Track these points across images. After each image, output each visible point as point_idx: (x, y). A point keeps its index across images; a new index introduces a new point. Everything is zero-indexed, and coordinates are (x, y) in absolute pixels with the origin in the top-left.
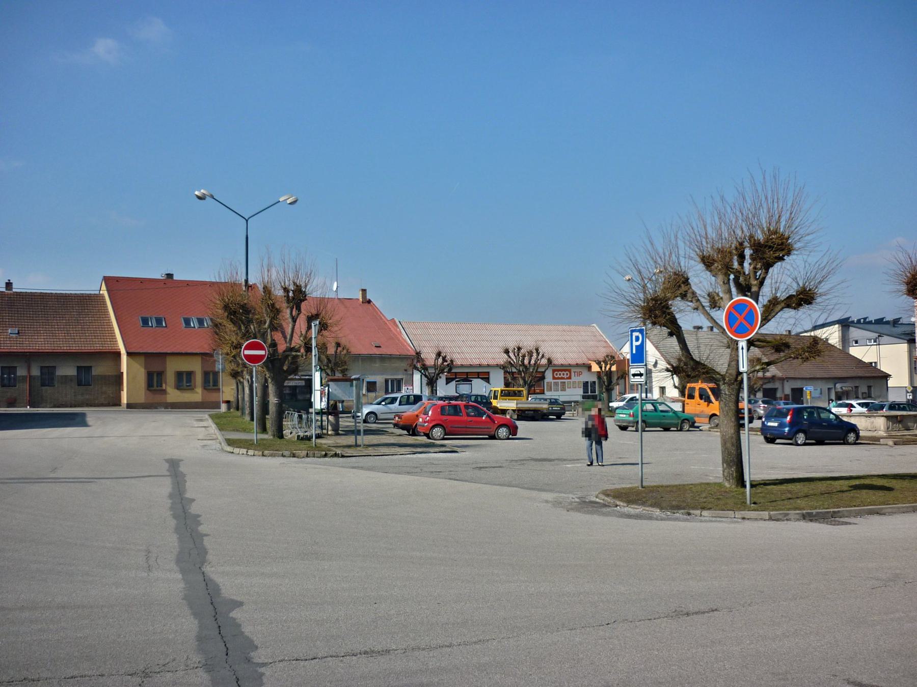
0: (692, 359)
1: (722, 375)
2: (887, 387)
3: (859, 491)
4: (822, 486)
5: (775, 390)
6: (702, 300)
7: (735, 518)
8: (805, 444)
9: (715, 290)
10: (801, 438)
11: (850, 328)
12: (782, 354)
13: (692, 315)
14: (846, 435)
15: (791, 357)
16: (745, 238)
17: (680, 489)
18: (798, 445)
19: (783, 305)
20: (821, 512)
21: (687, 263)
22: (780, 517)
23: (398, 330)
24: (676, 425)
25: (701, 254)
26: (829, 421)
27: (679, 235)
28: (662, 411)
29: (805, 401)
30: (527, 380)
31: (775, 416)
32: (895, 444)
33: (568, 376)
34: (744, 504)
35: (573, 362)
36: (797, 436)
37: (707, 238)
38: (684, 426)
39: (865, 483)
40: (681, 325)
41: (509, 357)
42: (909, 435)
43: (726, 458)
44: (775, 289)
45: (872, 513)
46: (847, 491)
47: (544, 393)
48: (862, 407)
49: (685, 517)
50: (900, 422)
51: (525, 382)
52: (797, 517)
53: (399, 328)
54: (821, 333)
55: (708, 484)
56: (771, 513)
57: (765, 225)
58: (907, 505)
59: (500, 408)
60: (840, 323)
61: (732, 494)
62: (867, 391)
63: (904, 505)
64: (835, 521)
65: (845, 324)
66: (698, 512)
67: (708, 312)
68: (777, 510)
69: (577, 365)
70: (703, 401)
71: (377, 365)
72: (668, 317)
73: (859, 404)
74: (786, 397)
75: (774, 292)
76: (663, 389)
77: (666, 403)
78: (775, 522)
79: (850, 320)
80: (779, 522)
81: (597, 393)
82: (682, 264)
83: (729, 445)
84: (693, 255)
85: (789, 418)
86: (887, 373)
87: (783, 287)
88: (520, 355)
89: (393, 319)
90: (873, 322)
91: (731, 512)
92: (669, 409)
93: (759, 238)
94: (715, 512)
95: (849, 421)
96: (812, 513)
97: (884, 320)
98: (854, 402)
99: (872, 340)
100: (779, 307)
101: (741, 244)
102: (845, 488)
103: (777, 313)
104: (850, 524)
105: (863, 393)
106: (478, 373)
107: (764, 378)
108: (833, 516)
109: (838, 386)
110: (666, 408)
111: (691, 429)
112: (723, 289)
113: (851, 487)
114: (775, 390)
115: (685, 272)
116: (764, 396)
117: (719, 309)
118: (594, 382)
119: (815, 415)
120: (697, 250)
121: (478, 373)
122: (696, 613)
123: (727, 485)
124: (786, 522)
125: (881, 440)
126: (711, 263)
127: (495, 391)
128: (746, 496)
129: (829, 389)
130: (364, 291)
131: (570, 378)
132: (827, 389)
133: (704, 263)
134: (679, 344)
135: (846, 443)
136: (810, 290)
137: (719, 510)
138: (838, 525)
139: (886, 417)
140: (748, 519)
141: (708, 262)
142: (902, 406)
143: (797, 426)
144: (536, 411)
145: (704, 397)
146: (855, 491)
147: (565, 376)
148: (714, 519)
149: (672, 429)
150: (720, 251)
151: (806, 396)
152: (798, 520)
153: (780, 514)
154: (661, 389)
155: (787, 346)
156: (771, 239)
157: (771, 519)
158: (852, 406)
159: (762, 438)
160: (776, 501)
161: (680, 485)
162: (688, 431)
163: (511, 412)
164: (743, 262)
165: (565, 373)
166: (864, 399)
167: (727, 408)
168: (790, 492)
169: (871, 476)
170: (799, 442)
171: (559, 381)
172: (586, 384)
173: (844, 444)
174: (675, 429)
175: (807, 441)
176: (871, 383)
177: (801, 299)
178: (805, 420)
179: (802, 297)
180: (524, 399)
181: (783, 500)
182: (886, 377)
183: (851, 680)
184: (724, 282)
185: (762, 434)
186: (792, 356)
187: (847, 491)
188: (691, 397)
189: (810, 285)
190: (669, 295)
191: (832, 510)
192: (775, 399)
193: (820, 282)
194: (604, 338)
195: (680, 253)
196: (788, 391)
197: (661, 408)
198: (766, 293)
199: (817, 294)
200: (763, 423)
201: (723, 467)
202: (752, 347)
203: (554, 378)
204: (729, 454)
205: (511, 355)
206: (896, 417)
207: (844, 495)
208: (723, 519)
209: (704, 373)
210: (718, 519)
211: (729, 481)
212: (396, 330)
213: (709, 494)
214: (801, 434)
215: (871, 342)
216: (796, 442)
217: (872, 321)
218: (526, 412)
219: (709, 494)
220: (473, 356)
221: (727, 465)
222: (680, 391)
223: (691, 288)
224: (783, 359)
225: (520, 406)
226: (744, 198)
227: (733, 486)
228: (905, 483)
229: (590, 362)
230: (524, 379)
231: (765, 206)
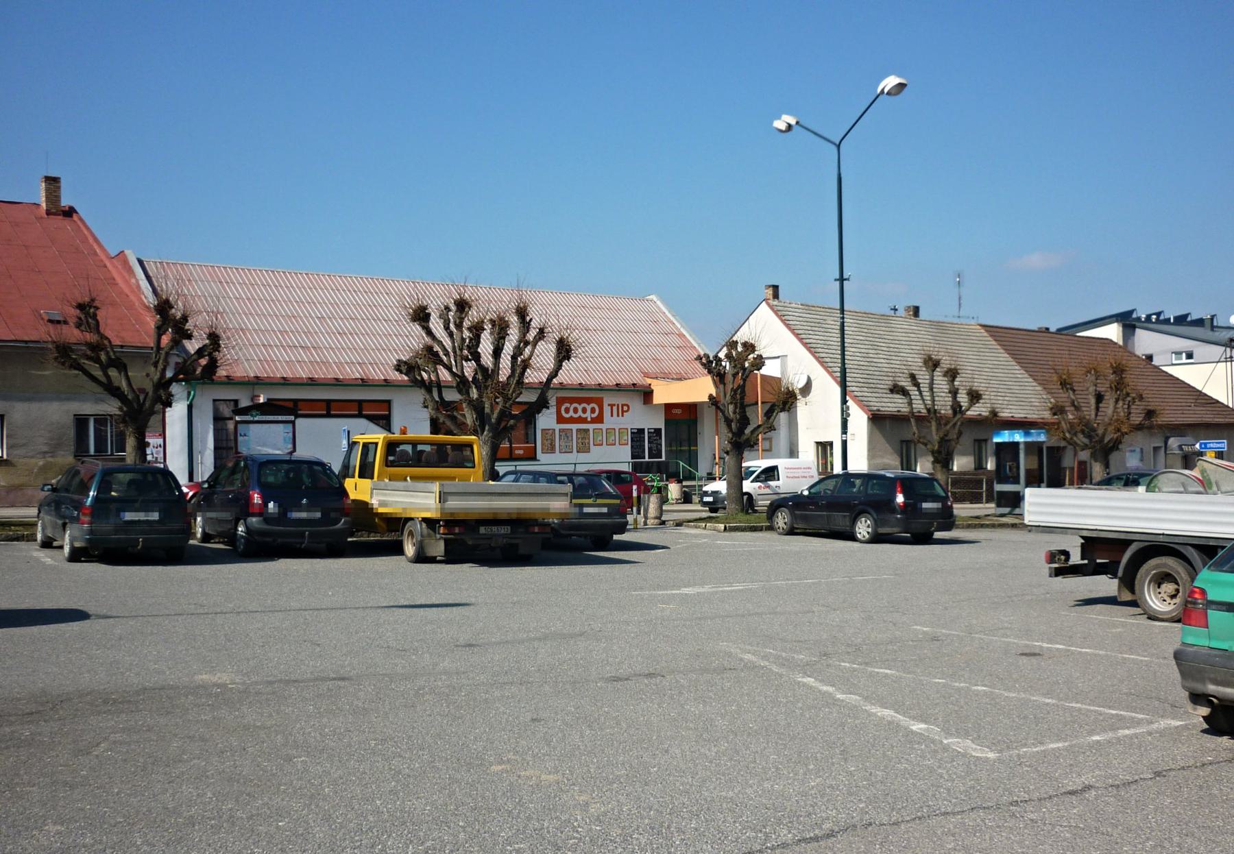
11: (1138, 331)
23: (133, 281)
30: (487, 410)
33: (594, 415)
35: (609, 381)
41: (429, 333)
47: (534, 458)
51: (482, 418)
53: (135, 276)
59: (381, 510)
60: (1121, 321)
69: (619, 388)
71: (47, 373)
79: (1134, 316)
81: (663, 459)
88: (466, 324)
89: (123, 252)
90: (1172, 321)
97: (1189, 319)
99: (1184, 355)
106: (360, 402)
118: (658, 431)
121: (360, 403)
127: (366, 446)
129: (1156, 449)
130: (52, 182)
131: (599, 419)
132: (1152, 449)
144: (519, 522)
147: (588, 415)
154: (977, 444)
163: (419, 528)
165: (589, 408)
171: (574, 427)
172: (638, 435)
180: (475, 476)
194: (677, 328)
203: (560, 419)
205: (436, 325)
212: (127, 282)
215: (1181, 359)
218: (482, 530)
220: (345, 357)
225: (454, 504)
229: (649, 381)
230: (477, 407)
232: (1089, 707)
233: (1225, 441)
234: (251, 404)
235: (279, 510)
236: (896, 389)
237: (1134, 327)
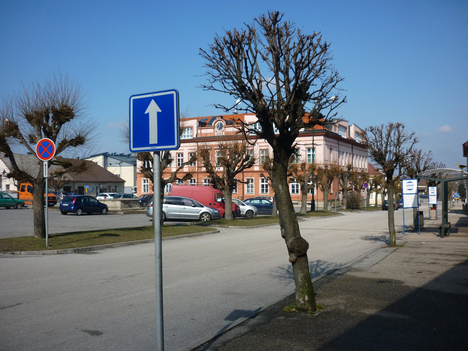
0: (19, 170)
1: (35, 179)
2: (124, 187)
3: (103, 237)
4: (86, 235)
5: (70, 187)
6: (25, 138)
7: (39, 254)
8: (82, 215)
9: (33, 133)
10: (80, 212)
11: (108, 157)
12: (68, 169)
13: (19, 146)
14: (102, 210)
15: (72, 171)
16: (49, 107)
17: (10, 240)
18: (78, 215)
19: (68, 143)
20: (83, 248)
21: (17, 117)
22: (63, 252)
24: (13, 206)
25: (26, 113)
26: (94, 203)
27: (13, 101)
28: (5, 198)
29: (85, 193)
31: (67, 201)
32: (124, 214)
34: (44, 247)
36: (78, 211)
37: (29, 105)
38: (18, 206)
39: (107, 233)
40: (12, 151)
42: (131, 209)
43: (36, 223)
44: (66, 135)
45: (108, 247)
46: (97, 237)
48: (111, 196)
49: (11, 255)
50: (127, 203)
52: (72, 251)
54: (95, 160)
55: (26, 237)
56: (58, 250)
57: (60, 102)
58: (124, 243)
61: (39, 242)
62: (115, 189)
63: (123, 243)
64: (90, 252)
65: (106, 155)
66: (18, 252)
67: (29, 145)
68: (62, 249)
70: (29, 193)
72: (5, 146)
73: (110, 195)
74: (76, 191)
75: (64, 137)
76: (8, 186)
77: (8, 194)
78: (60, 255)
79: (108, 153)
80: (62, 255)
82: (14, 118)
83: (38, 216)
84: (21, 113)
85: (74, 201)
87: (69, 135)
91: (37, 251)
92: (10, 197)
93: (57, 108)
94: (28, 252)
95: (104, 203)
96: (79, 249)
97: (124, 154)
98: (107, 194)
99: (118, 164)
100: (67, 145)
101: (47, 110)
102: (97, 236)
103: (65, 148)
104: (97, 253)
105: (113, 190)
107: (64, 181)
108: (90, 249)
109: (101, 186)
110: (8, 197)
111: (22, 208)
112: (37, 133)
113: (100, 235)
114: (70, 187)
115: (16, 122)
116: (64, 191)
117: (35, 144)
119: (87, 200)
120: (23, 111)
122: (9, 307)
123: (36, 237)
124: (65, 254)
125: (118, 212)
126: (31, 119)
128: (46, 242)
129: (97, 187)
133: (27, 118)
134: (11, 161)
135: (102, 214)
136: (82, 137)
137: (31, 250)
138: (91, 254)
139: (121, 201)
140: (46, 254)
141: (30, 118)
142: (129, 196)
143: (78, 206)
145: (30, 190)
146: (102, 237)
148: (27, 255)
149: (11, 208)
150: (36, 113)
151: (86, 190)
152: (72, 253)
153: (63, 250)
155: (70, 165)
156: (64, 109)
157: (58, 253)
158: (106, 196)
159: (60, 212)
160: (61, 244)
161: (10, 238)
162: (20, 209)
164: (49, 120)
166: (113, 192)
167: (37, 196)
168: (70, 239)
169: (110, 229)
170: (79, 214)
173: (101, 214)
174: (13, 208)
175: (83, 213)
176: (117, 184)
177: (78, 142)
178: (82, 203)
179: (78, 140)
181: (65, 243)
182: (123, 182)
183: (84, 329)
184: (38, 130)
185: (60, 210)
186: (73, 170)
187: (97, 237)
188: (23, 190)
189: (83, 135)
190: (6, 134)
191: (89, 247)
192: (70, 192)
193: (87, 134)
195: (13, 112)
196: (76, 188)
197: (5, 196)
198: (60, 137)
199: (86, 140)
200: (61, 204)
201: (34, 228)
202: (52, 165)
204: (38, 220)
206: (126, 201)
207: (96, 239)
208: (32, 255)
209: (25, 178)
210: (30, 255)
211: (37, 235)
213: (26, 242)
214: (79, 210)
216: (77, 214)
217: (118, 155)
219: (26, 242)
221: (36, 227)
222: (18, 187)
223: (19, 131)
224: (68, 171)
226: (50, 86)
227: (40, 238)
228: (125, 232)
231: (61, 91)
232: (90, 247)
233: (260, 194)
235: (463, 209)
236: (445, 165)
237: (107, 157)
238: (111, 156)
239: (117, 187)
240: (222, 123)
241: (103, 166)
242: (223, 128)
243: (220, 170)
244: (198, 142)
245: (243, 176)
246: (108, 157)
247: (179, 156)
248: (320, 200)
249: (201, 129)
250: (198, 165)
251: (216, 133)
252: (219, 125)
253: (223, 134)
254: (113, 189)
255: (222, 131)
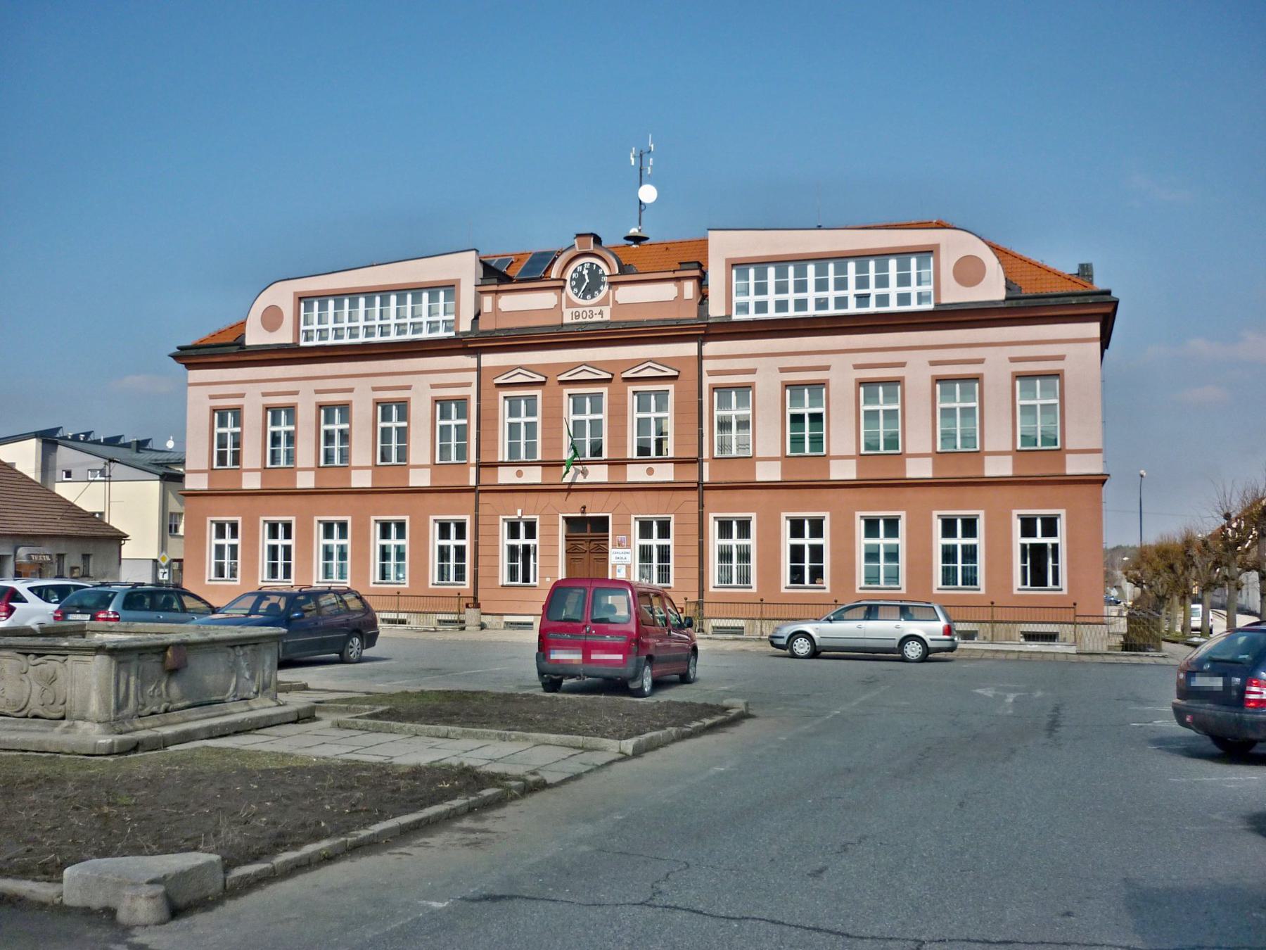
11: (60, 448)
48: (47, 600)
86: (120, 532)
90: (102, 441)
97: (122, 441)
105: (72, 569)
109: (23, 552)
182: (118, 538)
234: (76, 722)
237: (55, 444)
238: (71, 443)
239: (91, 560)
240: (598, 267)
241: (39, 474)
242: (605, 289)
243: (588, 480)
244: (477, 352)
245: (701, 505)
246: (59, 446)
247: (387, 417)
248: (1087, 620)
249: (497, 292)
250: (478, 455)
251: (571, 310)
252: (581, 275)
253: (601, 313)
254: (73, 565)
255: (604, 302)
